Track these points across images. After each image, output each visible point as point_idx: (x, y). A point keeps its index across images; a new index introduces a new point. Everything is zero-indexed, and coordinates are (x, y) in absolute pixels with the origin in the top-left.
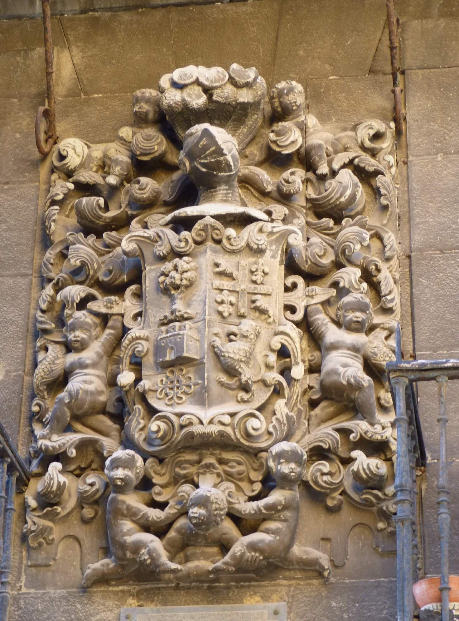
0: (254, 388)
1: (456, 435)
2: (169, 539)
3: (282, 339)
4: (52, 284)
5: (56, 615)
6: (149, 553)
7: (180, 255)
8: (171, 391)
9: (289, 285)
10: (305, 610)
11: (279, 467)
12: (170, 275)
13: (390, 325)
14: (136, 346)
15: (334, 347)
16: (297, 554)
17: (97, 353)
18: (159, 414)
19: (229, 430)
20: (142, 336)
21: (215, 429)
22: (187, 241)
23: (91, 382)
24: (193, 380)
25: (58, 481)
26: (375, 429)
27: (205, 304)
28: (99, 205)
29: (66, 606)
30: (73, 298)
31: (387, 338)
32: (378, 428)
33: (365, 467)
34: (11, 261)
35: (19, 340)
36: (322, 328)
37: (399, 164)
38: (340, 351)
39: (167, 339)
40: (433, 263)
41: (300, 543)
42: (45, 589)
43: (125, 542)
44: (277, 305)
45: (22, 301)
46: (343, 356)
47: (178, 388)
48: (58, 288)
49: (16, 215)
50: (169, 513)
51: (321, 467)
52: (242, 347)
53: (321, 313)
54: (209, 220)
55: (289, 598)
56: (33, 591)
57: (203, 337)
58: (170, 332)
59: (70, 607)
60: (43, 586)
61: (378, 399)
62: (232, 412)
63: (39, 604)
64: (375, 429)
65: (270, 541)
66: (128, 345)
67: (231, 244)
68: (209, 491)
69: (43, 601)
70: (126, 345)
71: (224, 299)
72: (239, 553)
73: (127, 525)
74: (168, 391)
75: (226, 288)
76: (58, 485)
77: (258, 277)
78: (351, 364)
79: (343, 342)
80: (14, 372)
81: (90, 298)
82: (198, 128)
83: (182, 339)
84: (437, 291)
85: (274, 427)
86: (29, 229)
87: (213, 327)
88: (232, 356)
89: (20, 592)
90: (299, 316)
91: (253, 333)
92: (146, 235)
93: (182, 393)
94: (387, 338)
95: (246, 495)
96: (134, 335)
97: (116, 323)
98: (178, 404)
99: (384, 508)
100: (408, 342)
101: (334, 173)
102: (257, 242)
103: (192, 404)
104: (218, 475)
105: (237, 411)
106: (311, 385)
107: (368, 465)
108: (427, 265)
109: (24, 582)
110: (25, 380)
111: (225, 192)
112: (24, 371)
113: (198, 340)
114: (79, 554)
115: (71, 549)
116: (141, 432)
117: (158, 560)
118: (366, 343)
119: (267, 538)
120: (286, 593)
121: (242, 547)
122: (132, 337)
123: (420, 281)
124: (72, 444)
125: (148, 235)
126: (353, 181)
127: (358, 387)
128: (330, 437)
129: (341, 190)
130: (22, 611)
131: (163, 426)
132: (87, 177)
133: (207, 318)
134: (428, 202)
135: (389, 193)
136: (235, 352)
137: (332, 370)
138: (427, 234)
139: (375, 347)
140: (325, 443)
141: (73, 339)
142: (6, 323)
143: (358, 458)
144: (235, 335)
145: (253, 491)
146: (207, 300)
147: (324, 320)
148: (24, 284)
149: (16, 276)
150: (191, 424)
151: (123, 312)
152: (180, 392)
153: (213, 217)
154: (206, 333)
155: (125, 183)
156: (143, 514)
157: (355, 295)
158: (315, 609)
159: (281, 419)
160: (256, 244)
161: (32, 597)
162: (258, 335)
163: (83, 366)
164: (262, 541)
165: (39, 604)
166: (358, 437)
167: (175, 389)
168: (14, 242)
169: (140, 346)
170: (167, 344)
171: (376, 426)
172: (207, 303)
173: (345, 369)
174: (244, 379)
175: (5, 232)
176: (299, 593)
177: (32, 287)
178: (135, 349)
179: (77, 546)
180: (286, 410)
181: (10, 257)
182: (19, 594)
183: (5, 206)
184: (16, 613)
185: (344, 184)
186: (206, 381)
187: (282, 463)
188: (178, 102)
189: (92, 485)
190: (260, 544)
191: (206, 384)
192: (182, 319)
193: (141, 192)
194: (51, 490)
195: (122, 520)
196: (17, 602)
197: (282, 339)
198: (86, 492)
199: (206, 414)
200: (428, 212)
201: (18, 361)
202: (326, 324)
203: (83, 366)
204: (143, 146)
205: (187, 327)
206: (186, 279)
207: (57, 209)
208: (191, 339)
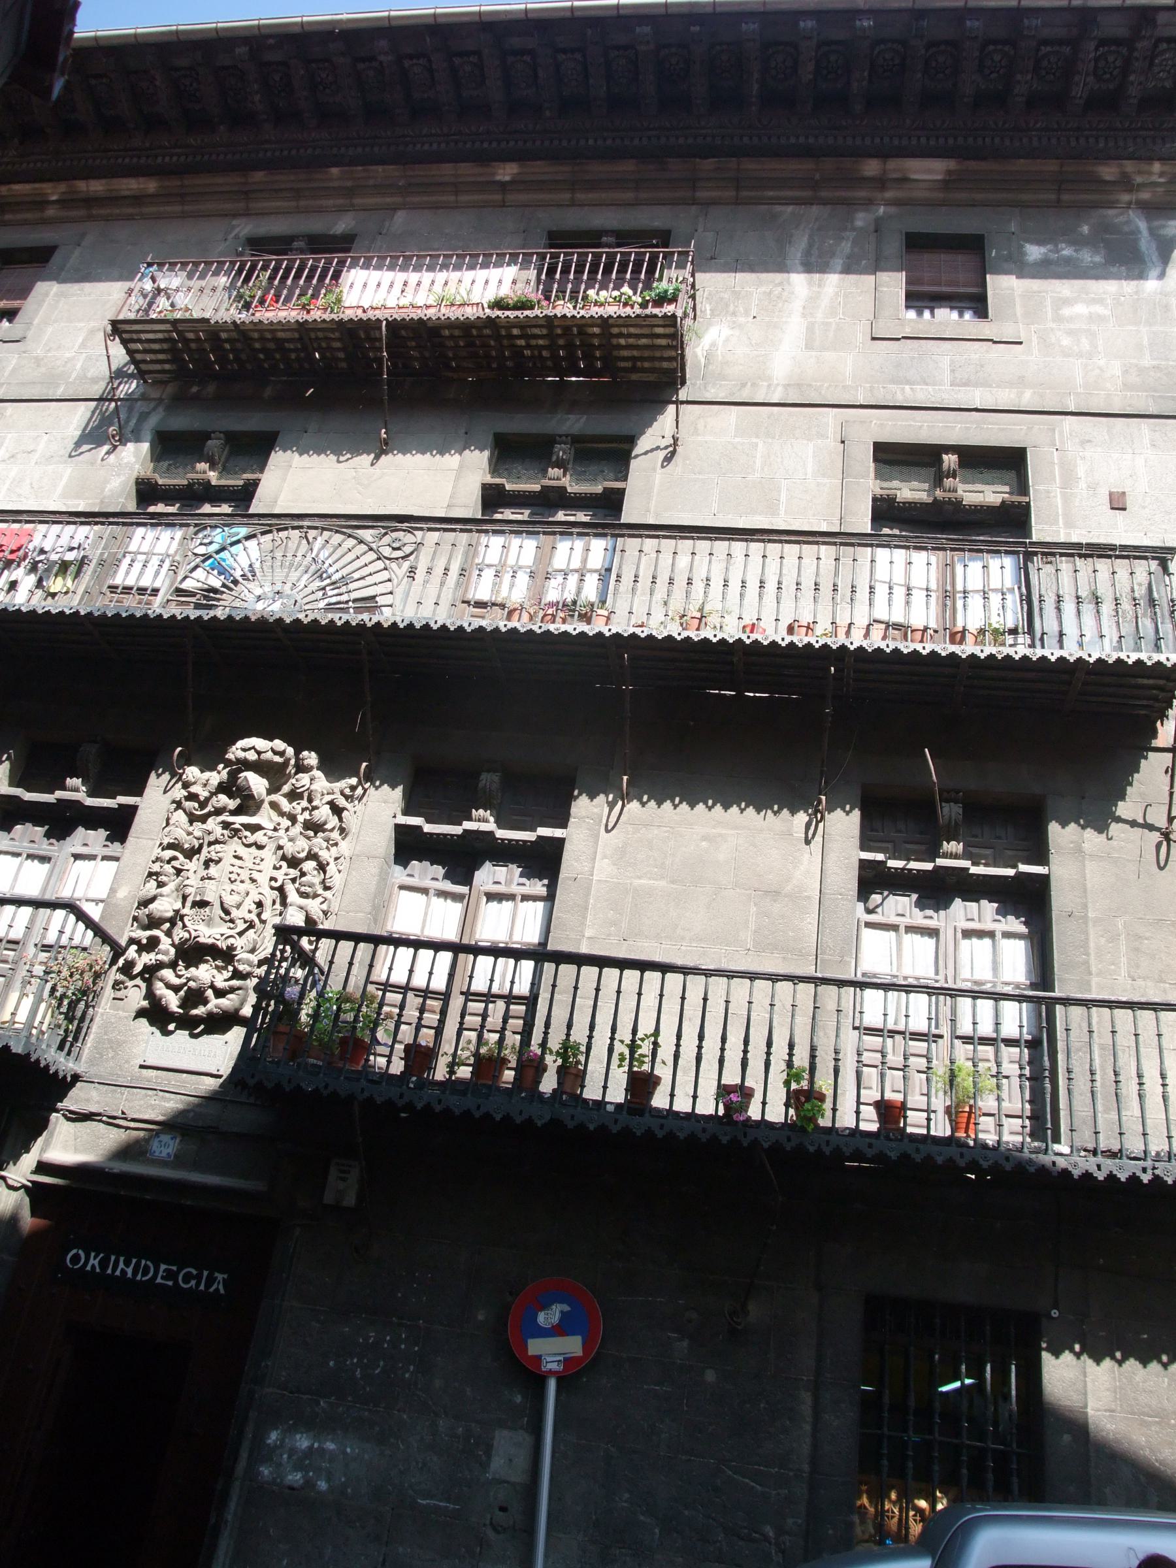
21: (210, 941)
54: (237, 826)
60: (118, 1010)
81: (175, 858)
162: (248, 894)
163: (161, 895)
203: (161, 895)
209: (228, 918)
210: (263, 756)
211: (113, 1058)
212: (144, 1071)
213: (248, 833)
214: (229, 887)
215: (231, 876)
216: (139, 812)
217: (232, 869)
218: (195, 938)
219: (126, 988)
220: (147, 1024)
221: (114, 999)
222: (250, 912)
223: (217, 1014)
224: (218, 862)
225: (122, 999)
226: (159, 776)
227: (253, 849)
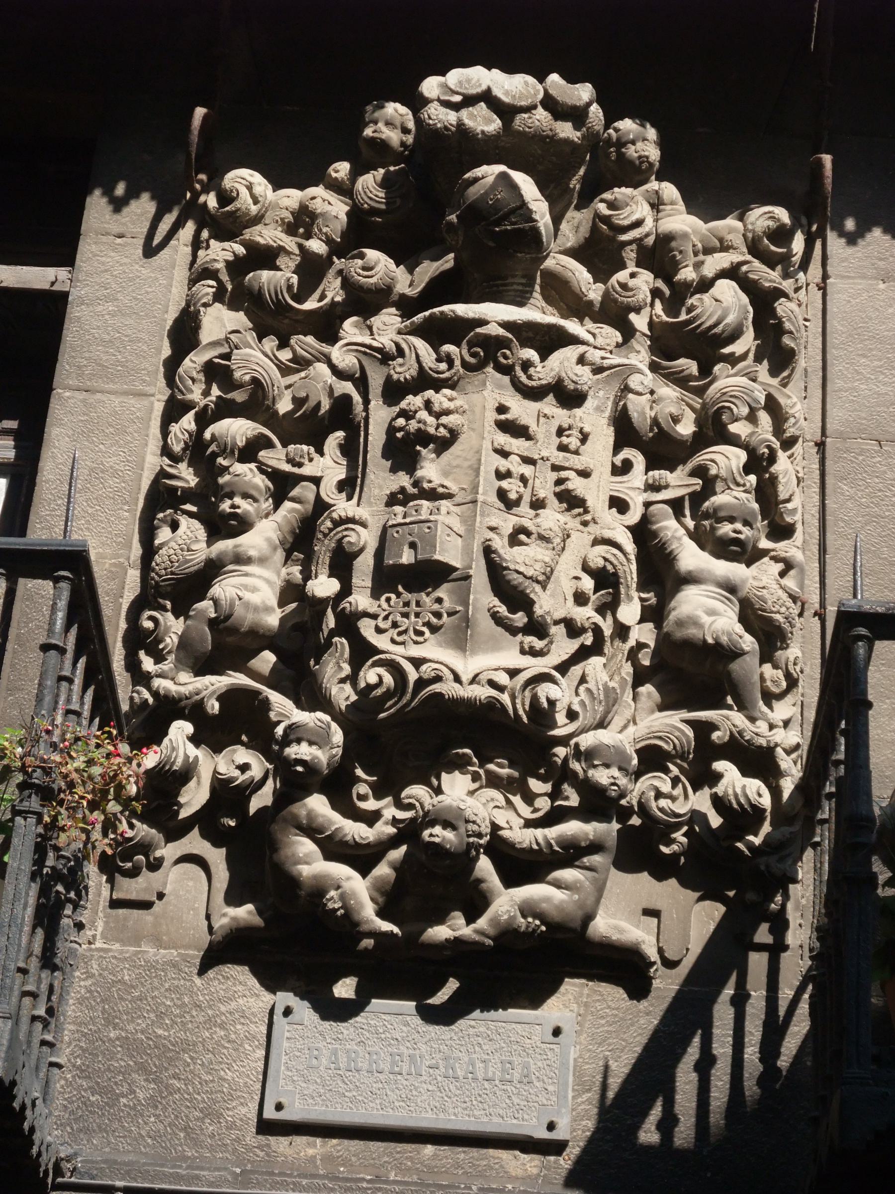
0: (553, 630)
1: (890, 756)
2: (376, 878)
3: (607, 552)
4: (193, 412)
5: (156, 993)
6: (342, 897)
7: (438, 385)
8: (405, 620)
9: (618, 463)
10: (607, 1032)
11: (591, 773)
12: (418, 415)
13: (788, 554)
14: (345, 533)
15: (690, 579)
16: (601, 930)
17: (269, 540)
18: (381, 656)
19: (505, 698)
20: (357, 517)
21: (482, 692)
22: (450, 363)
23: (254, 590)
24: (447, 604)
25: (185, 754)
26: (758, 727)
27: (478, 475)
28: (290, 287)
29: (174, 979)
30: (234, 438)
31: (782, 574)
32: (762, 726)
33: (739, 791)
34: (119, 368)
35: (124, 504)
36: (671, 544)
37: (809, 287)
38: (703, 587)
39: (405, 527)
40: (864, 460)
41: (605, 912)
42: (140, 947)
43: (300, 874)
44: (601, 493)
45: (133, 438)
46: (708, 597)
47: (417, 615)
48: (204, 419)
49: (133, 291)
50: (383, 832)
51: (657, 783)
52: (539, 557)
53: (671, 518)
54: (494, 330)
55: (579, 1006)
56: (117, 946)
57: (471, 530)
58: (412, 516)
59: (182, 982)
60: (136, 940)
61: (762, 678)
62: (512, 667)
63: (125, 972)
64: (758, 727)
65: (562, 901)
66: (331, 530)
67: (530, 377)
68: (463, 801)
69: (134, 966)
70: (327, 531)
71: (512, 469)
72: (506, 917)
73: (305, 846)
74: (399, 618)
75: (516, 451)
76: (184, 761)
77: (573, 442)
78: (722, 611)
79: (709, 572)
80: (110, 559)
82: (490, 172)
83: (432, 530)
84: (867, 507)
85: (582, 703)
86: (155, 317)
87: (488, 515)
88: (521, 569)
89: (93, 946)
90: (634, 516)
91: (561, 535)
92: (375, 344)
93: (424, 624)
94: (782, 574)
95: (519, 815)
96: (343, 514)
97: (306, 493)
98: (416, 643)
99: (763, 868)
100: (812, 589)
101: (705, 285)
102: (575, 378)
103: (441, 646)
104: (475, 777)
105: (522, 667)
106: (642, 640)
107: (744, 787)
108: (852, 462)
109: (100, 929)
110: (129, 574)
111: (520, 288)
112: (128, 559)
113: (461, 536)
114: (207, 888)
115: (192, 879)
116: (342, 685)
117: (359, 914)
118: (747, 579)
119: (558, 895)
120: (575, 998)
121: (512, 906)
122: (340, 517)
123: (839, 488)
124: (214, 692)
125: (381, 346)
126: (739, 300)
127: (735, 654)
128: (677, 734)
129: (719, 313)
130: (93, 980)
131: (388, 680)
132: (268, 239)
133: (480, 498)
134: (859, 355)
135: (797, 331)
136: (527, 563)
137: (689, 617)
138: (855, 410)
139: (764, 588)
140: (667, 742)
141: (228, 510)
142: (102, 472)
143: (725, 774)
144: (528, 534)
145: (536, 810)
146: (482, 468)
147: (676, 530)
148: (139, 409)
149: (126, 393)
150: (438, 679)
151: (319, 474)
152: (420, 622)
153: (500, 325)
154: (477, 524)
155: (335, 259)
156: (337, 829)
157: (735, 493)
158: (625, 1033)
159: (595, 692)
160: (573, 382)
161: (115, 957)
163: (241, 559)
164: (547, 899)
165: (125, 972)
166: (727, 738)
167: (412, 617)
168: (126, 336)
169: (352, 533)
170: (403, 536)
171: (758, 723)
172: (482, 473)
173: (712, 618)
174: (538, 610)
175: (113, 316)
176: (598, 1001)
177: (153, 417)
178: (347, 536)
179: (202, 874)
180: (604, 677)
181: (118, 361)
182: (91, 950)
183: (115, 273)
184: (82, 983)
185: (725, 304)
186: (471, 607)
187: (597, 765)
188: (451, 125)
189: (244, 768)
190: (544, 905)
191: (470, 613)
192: (433, 495)
193: (366, 273)
194: (169, 769)
195: (297, 835)
196: (86, 963)
197: (607, 552)
198: (231, 780)
199: (467, 666)
200: (858, 373)
201: (120, 539)
202: (679, 539)
203: (241, 559)
204: (376, 196)
205: (443, 510)
206: (445, 427)
207: (212, 287)
208: (449, 531)
209: (520, 619)
210: (520, 121)
211: (153, 1102)
212: (281, 1144)
213: (530, 354)
214: (507, 523)
215: (505, 484)
216: (75, 312)
217: (503, 464)
218: (421, 683)
219: (155, 865)
220: (253, 982)
221: (115, 904)
222: (580, 599)
223: (530, 934)
224: (443, 444)
225: (146, 905)
226: (118, 205)
227: (549, 406)
